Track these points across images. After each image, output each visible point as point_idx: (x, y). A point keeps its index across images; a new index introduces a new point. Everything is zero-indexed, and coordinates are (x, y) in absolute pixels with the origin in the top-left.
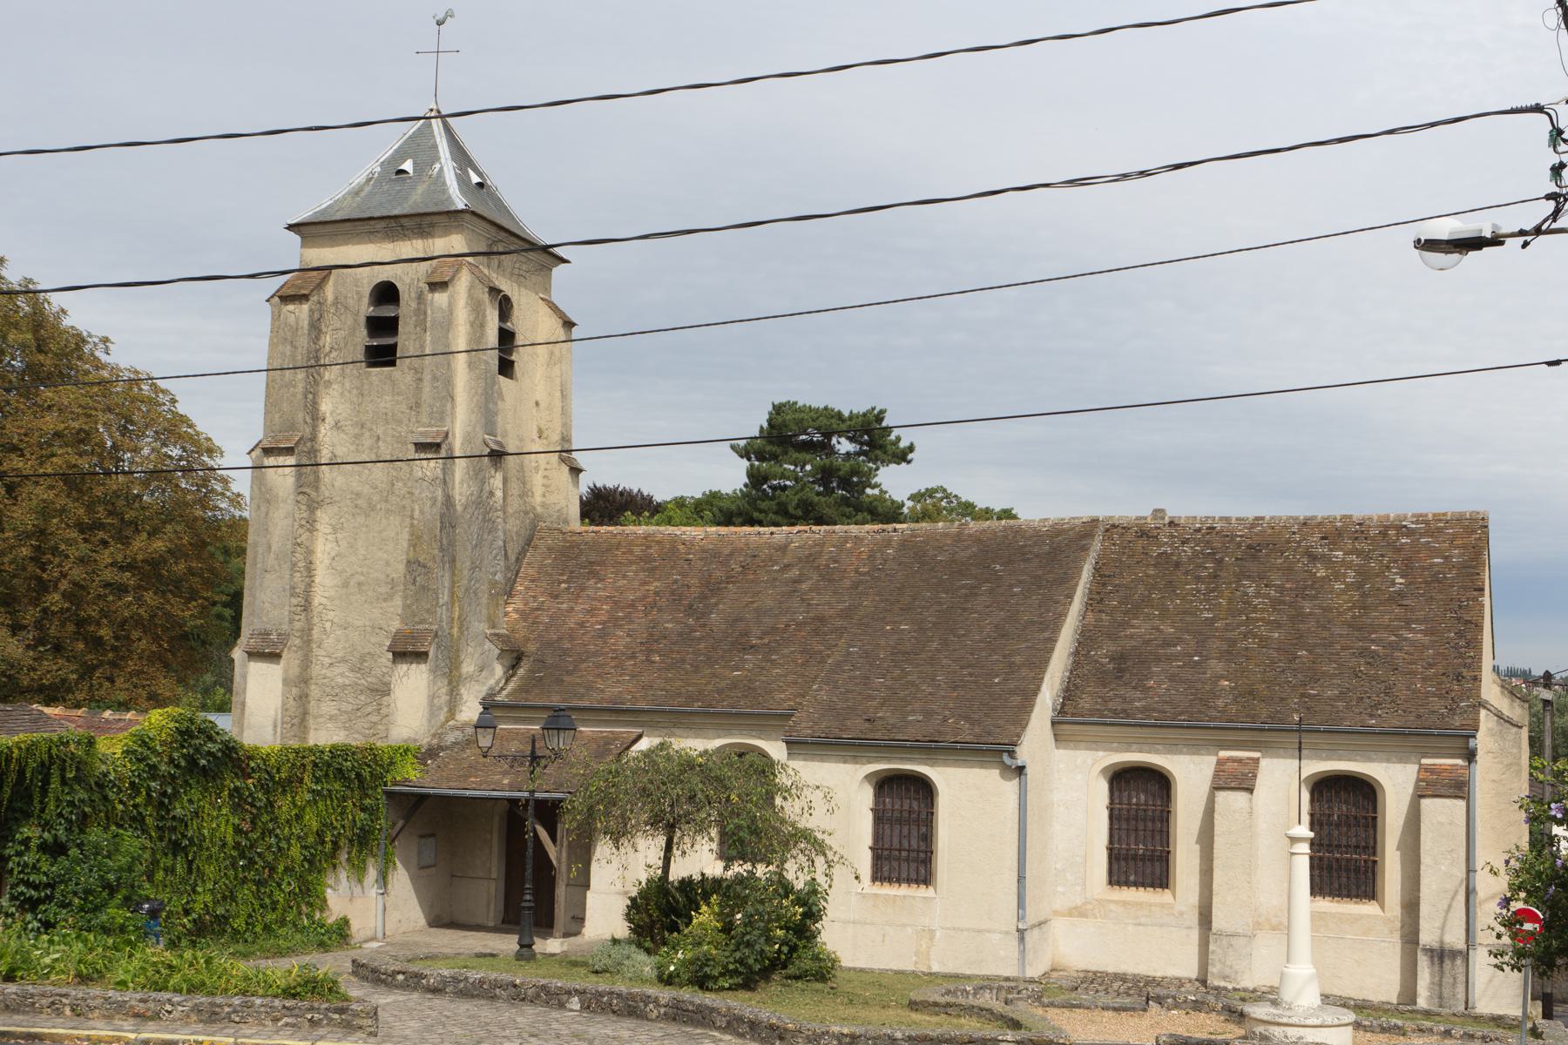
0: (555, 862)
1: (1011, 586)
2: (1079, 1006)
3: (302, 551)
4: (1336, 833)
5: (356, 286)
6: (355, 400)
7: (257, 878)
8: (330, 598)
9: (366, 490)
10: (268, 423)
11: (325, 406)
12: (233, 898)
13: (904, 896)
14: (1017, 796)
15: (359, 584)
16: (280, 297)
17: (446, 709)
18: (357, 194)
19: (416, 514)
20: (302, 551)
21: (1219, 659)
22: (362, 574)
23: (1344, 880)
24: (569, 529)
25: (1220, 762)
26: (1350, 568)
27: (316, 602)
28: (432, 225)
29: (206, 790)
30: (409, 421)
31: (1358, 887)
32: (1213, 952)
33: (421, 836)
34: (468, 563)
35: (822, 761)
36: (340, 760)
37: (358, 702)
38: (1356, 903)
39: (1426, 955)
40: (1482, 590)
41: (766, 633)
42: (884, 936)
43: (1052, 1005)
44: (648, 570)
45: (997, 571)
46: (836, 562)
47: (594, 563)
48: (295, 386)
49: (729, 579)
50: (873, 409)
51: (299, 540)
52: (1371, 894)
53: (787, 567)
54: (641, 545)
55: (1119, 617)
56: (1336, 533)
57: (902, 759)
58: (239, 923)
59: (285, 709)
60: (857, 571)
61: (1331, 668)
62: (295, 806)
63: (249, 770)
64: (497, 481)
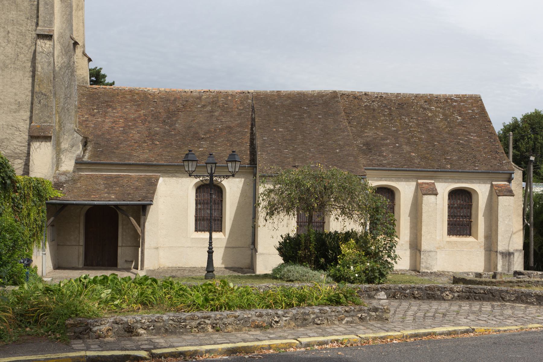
0: (140, 234)
30: (27, 24)
34: (63, 96)
39: (501, 255)
47: (108, 101)
53: (204, 106)
54: (130, 95)
56: (430, 100)
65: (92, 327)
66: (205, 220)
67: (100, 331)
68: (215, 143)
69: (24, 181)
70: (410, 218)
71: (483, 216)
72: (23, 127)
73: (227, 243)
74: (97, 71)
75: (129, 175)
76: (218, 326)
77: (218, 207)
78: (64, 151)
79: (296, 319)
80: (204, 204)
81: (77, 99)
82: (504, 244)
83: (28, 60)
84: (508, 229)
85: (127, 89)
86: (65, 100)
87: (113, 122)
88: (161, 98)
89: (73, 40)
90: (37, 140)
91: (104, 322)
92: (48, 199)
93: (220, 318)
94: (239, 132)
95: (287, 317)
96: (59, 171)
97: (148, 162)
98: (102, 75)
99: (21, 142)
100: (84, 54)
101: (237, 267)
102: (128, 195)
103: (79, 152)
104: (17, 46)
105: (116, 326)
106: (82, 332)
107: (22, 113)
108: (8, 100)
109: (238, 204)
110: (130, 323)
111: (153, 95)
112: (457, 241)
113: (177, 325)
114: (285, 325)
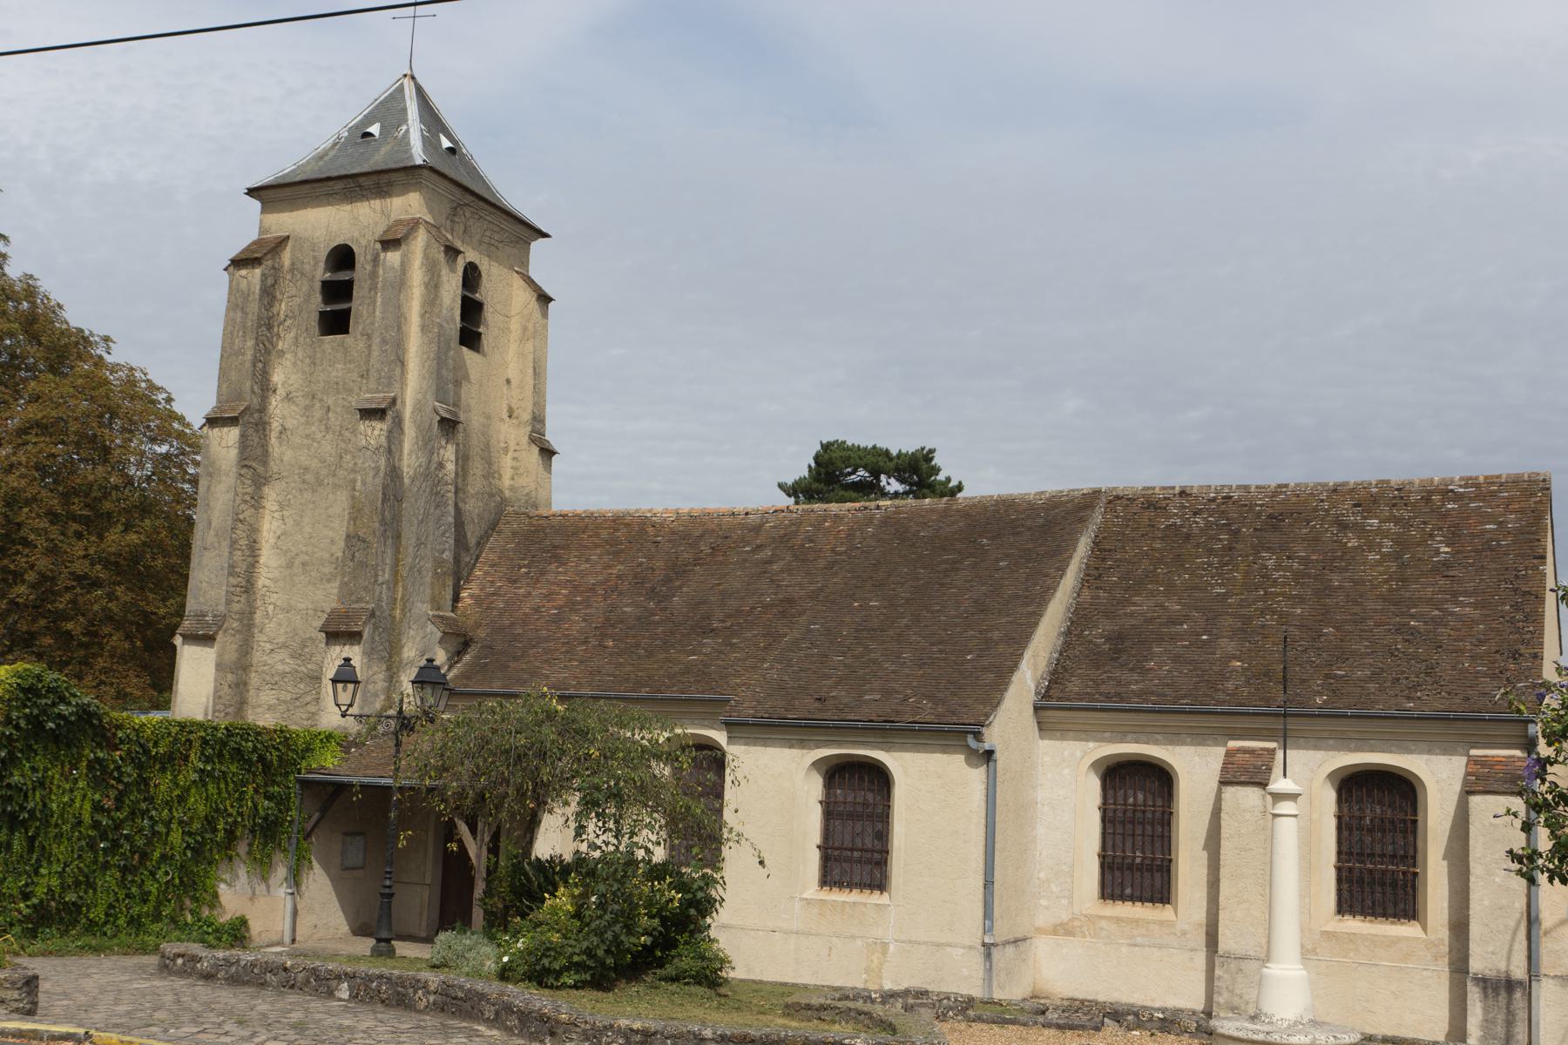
0: (474, 861)
1: (997, 560)
2: (1013, 1022)
3: (246, 528)
4: (1368, 839)
5: (314, 251)
6: (307, 369)
7: (122, 863)
8: (275, 580)
9: (315, 464)
11: (277, 377)
12: (91, 885)
13: (854, 903)
14: (984, 786)
15: (304, 564)
17: (382, 697)
19: (359, 485)
20: (246, 528)
21: (1231, 638)
22: (307, 553)
23: (1378, 896)
24: (537, 512)
25: (1229, 754)
26: (1387, 537)
27: (260, 583)
28: (390, 184)
29: (57, 758)
31: (1396, 904)
32: (1219, 978)
33: (346, 834)
34: (414, 540)
35: (765, 745)
36: (238, 739)
37: (298, 691)
38: (1393, 923)
40: (1543, 557)
41: (729, 616)
42: (831, 948)
43: (979, 1019)
44: (613, 553)
45: (983, 545)
46: (811, 541)
47: (557, 547)
48: (243, 354)
49: (697, 561)
50: (923, 449)
51: (241, 517)
52: (1411, 913)
53: (760, 547)
54: (610, 528)
55: (1118, 593)
56: (1369, 499)
57: (854, 742)
58: (97, 913)
59: (217, 695)
60: (833, 551)
61: (1362, 647)
62: (177, 785)
63: (117, 741)
64: (449, 453)
70: (1209, 854)
71: (1444, 859)
82: (1490, 949)
84: (1504, 902)
85: (610, 515)
92: (303, 771)
112: (1354, 934)
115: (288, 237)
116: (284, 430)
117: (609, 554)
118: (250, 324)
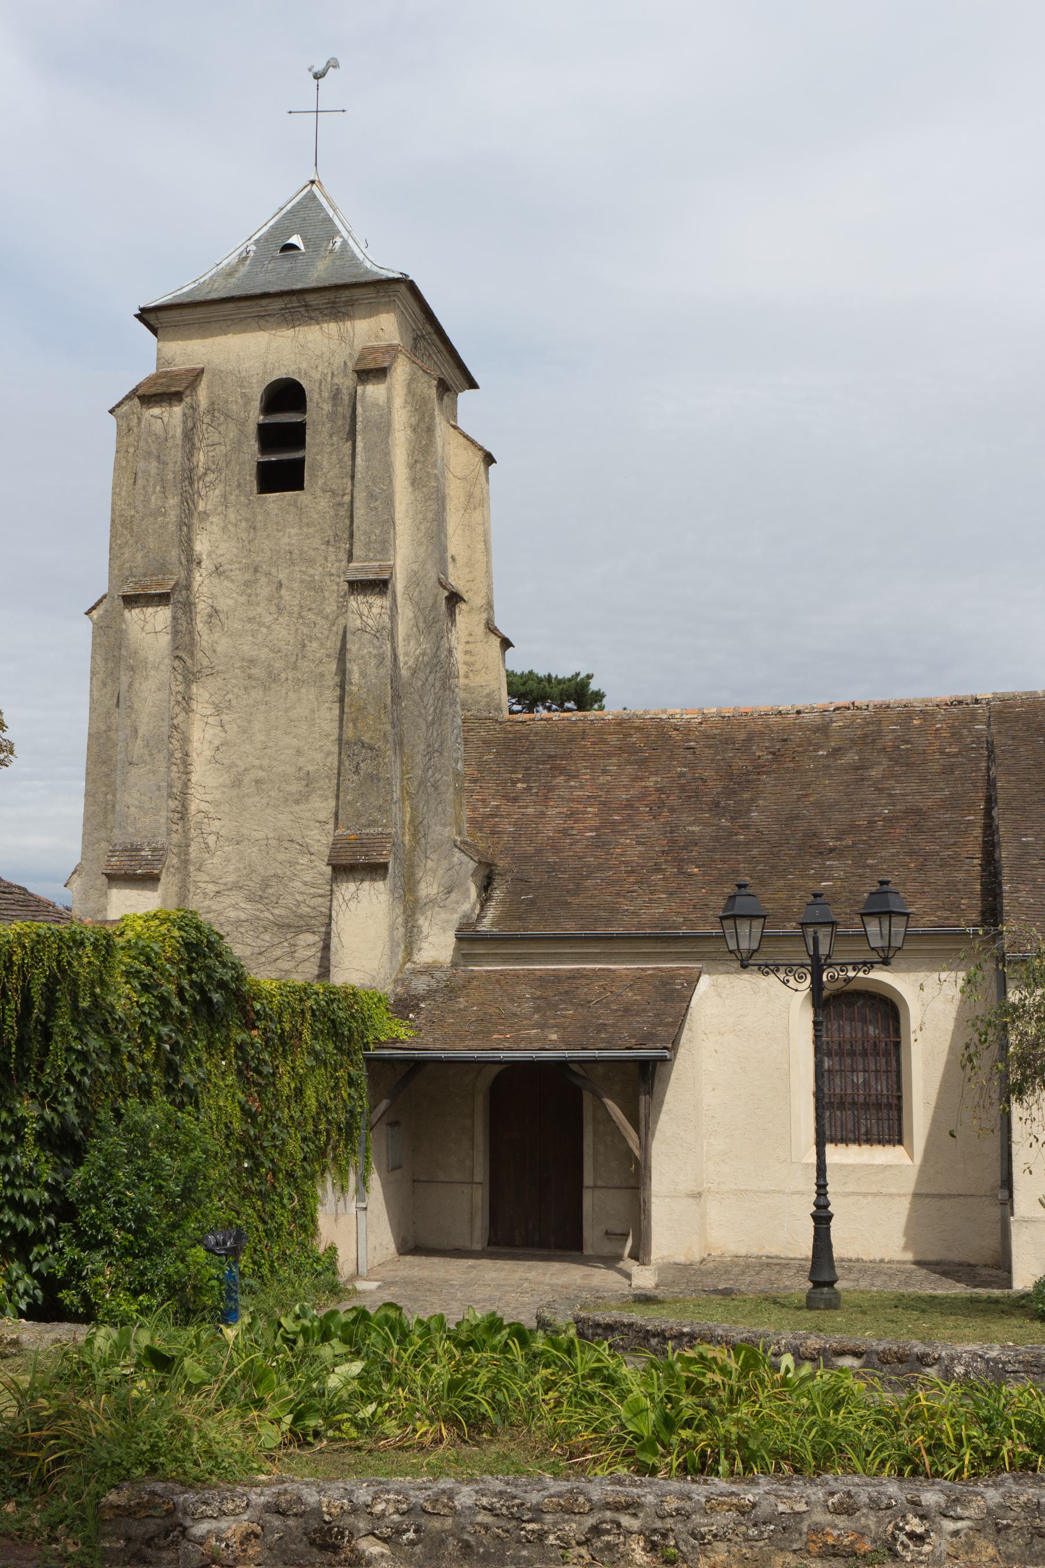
5: (241, 387)
6: (244, 535)
8: (215, 803)
9: (264, 654)
10: (116, 572)
11: (201, 546)
15: (258, 782)
16: (139, 397)
18: (230, 274)
22: (261, 768)
27: (193, 808)
28: (351, 303)
30: (326, 559)
34: (422, 747)
44: (636, 762)
46: (907, 742)
47: (555, 756)
48: (164, 515)
49: (759, 769)
51: (175, 722)
53: (836, 752)
54: (617, 733)
65: (188, 1522)
66: (847, 1106)
67: (219, 1539)
68: (870, 862)
69: (281, 995)
72: (319, 841)
73: (919, 1182)
74: (577, 684)
75: (609, 970)
76: (672, 1543)
77: (886, 1063)
78: (425, 904)
79: (999, 1531)
80: (840, 1053)
81: (460, 754)
83: (328, 656)
85: (610, 717)
86: (427, 758)
87: (567, 816)
88: (708, 737)
89: (445, 588)
90: (351, 877)
91: (231, 1506)
92: (372, 1047)
93: (677, 1510)
94: (947, 825)
95: (961, 1519)
96: (414, 963)
97: (665, 928)
98: (592, 693)
99: (313, 885)
100: (489, 629)
101: (956, 1259)
102: (599, 1032)
103: (466, 907)
104: (301, 621)
105: (277, 1523)
106: (152, 1538)
107: (316, 802)
108: (281, 769)
109: (949, 1054)
110: (330, 1514)
111: (685, 729)
113: (507, 1531)
114: (951, 1550)
115: (202, 371)
116: (215, 612)
117: (631, 764)
118: (171, 476)
